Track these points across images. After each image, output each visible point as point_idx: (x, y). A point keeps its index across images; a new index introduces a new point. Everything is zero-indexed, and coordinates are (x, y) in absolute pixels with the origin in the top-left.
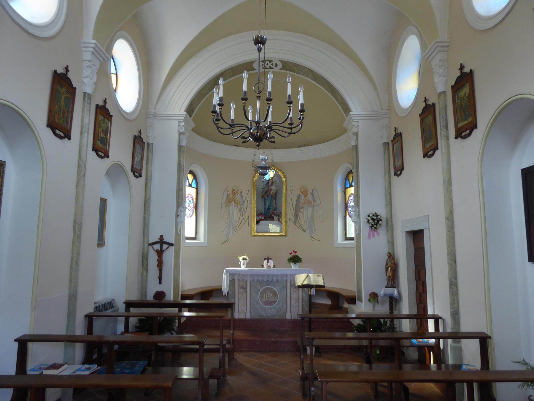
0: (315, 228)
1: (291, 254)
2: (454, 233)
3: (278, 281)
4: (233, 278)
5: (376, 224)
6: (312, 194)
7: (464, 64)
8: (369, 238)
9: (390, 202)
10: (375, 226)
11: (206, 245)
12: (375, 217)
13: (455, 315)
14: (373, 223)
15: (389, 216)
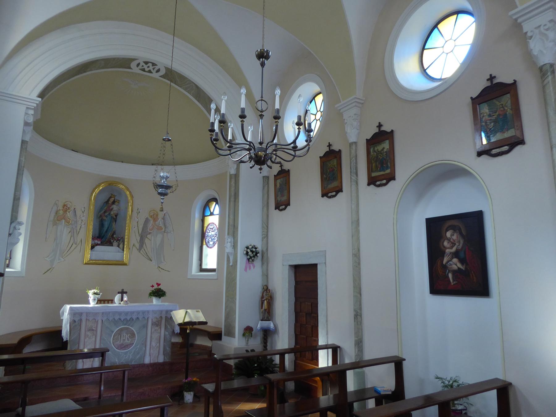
0: (164, 257)
1: (153, 286)
2: (360, 269)
3: (132, 319)
4: (77, 318)
5: (254, 257)
6: (163, 219)
7: (382, 124)
8: (246, 270)
9: (267, 235)
10: (253, 258)
11: (24, 275)
12: (254, 250)
13: (359, 344)
14: (252, 256)
15: (265, 250)
